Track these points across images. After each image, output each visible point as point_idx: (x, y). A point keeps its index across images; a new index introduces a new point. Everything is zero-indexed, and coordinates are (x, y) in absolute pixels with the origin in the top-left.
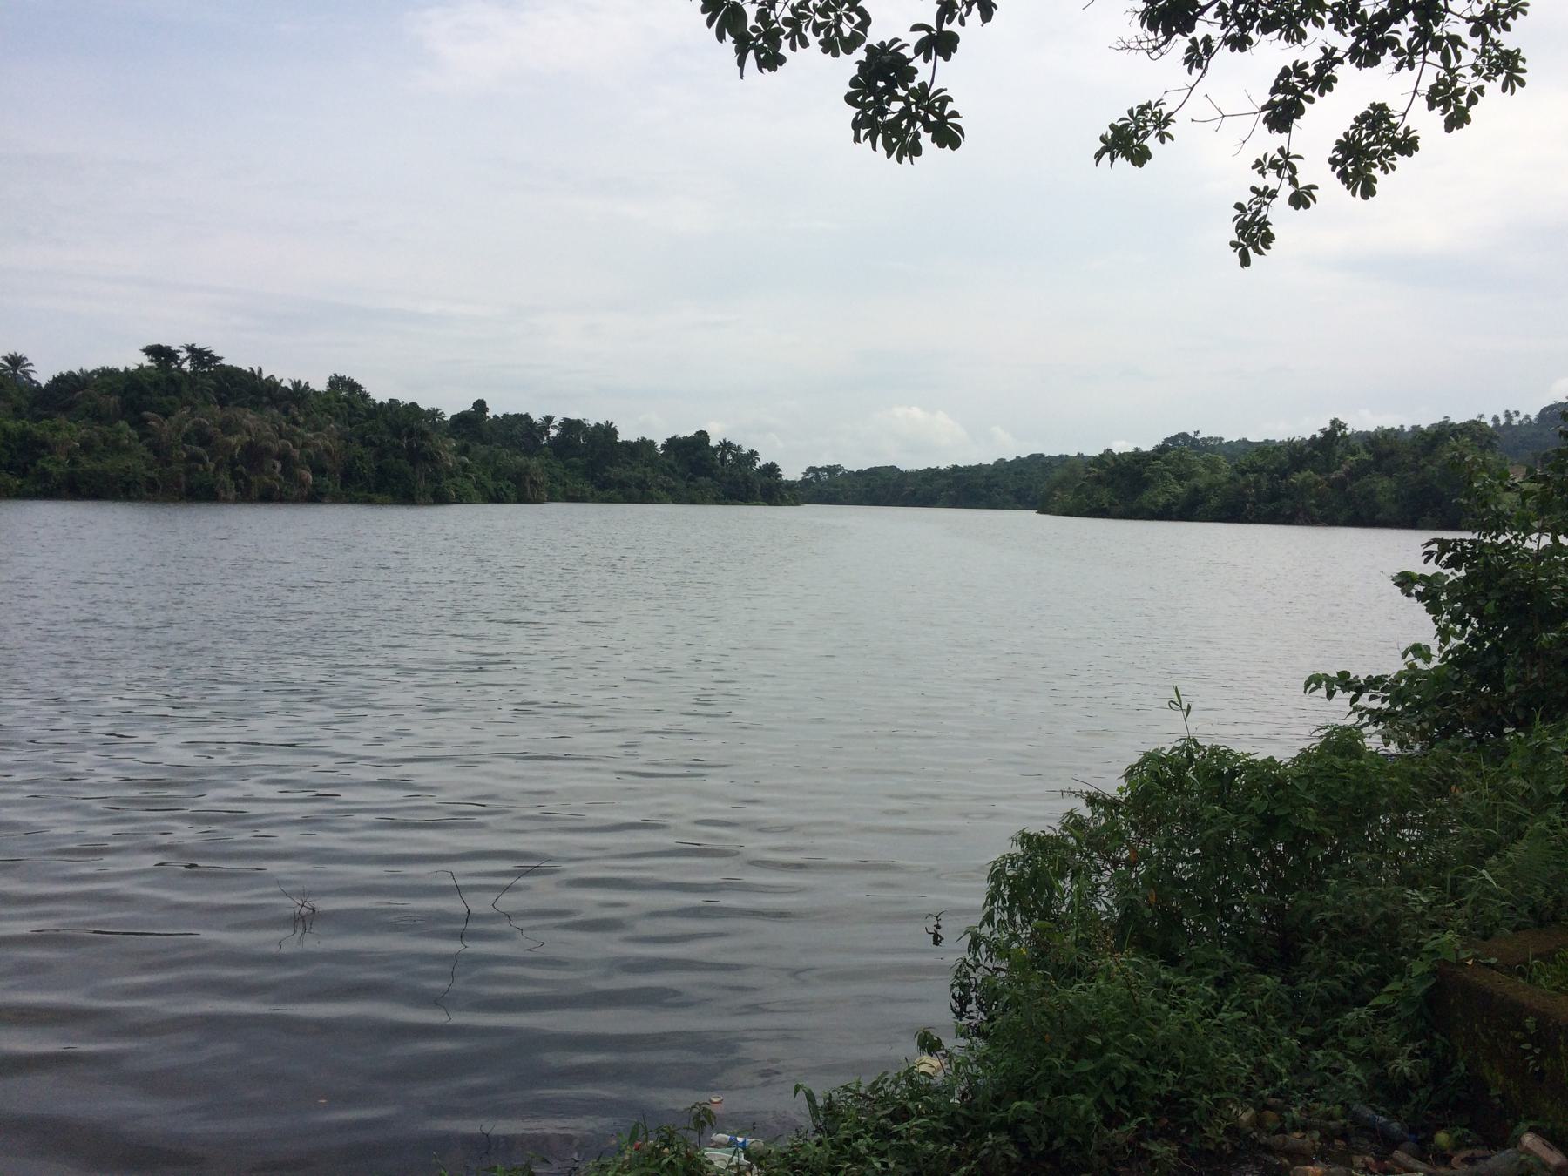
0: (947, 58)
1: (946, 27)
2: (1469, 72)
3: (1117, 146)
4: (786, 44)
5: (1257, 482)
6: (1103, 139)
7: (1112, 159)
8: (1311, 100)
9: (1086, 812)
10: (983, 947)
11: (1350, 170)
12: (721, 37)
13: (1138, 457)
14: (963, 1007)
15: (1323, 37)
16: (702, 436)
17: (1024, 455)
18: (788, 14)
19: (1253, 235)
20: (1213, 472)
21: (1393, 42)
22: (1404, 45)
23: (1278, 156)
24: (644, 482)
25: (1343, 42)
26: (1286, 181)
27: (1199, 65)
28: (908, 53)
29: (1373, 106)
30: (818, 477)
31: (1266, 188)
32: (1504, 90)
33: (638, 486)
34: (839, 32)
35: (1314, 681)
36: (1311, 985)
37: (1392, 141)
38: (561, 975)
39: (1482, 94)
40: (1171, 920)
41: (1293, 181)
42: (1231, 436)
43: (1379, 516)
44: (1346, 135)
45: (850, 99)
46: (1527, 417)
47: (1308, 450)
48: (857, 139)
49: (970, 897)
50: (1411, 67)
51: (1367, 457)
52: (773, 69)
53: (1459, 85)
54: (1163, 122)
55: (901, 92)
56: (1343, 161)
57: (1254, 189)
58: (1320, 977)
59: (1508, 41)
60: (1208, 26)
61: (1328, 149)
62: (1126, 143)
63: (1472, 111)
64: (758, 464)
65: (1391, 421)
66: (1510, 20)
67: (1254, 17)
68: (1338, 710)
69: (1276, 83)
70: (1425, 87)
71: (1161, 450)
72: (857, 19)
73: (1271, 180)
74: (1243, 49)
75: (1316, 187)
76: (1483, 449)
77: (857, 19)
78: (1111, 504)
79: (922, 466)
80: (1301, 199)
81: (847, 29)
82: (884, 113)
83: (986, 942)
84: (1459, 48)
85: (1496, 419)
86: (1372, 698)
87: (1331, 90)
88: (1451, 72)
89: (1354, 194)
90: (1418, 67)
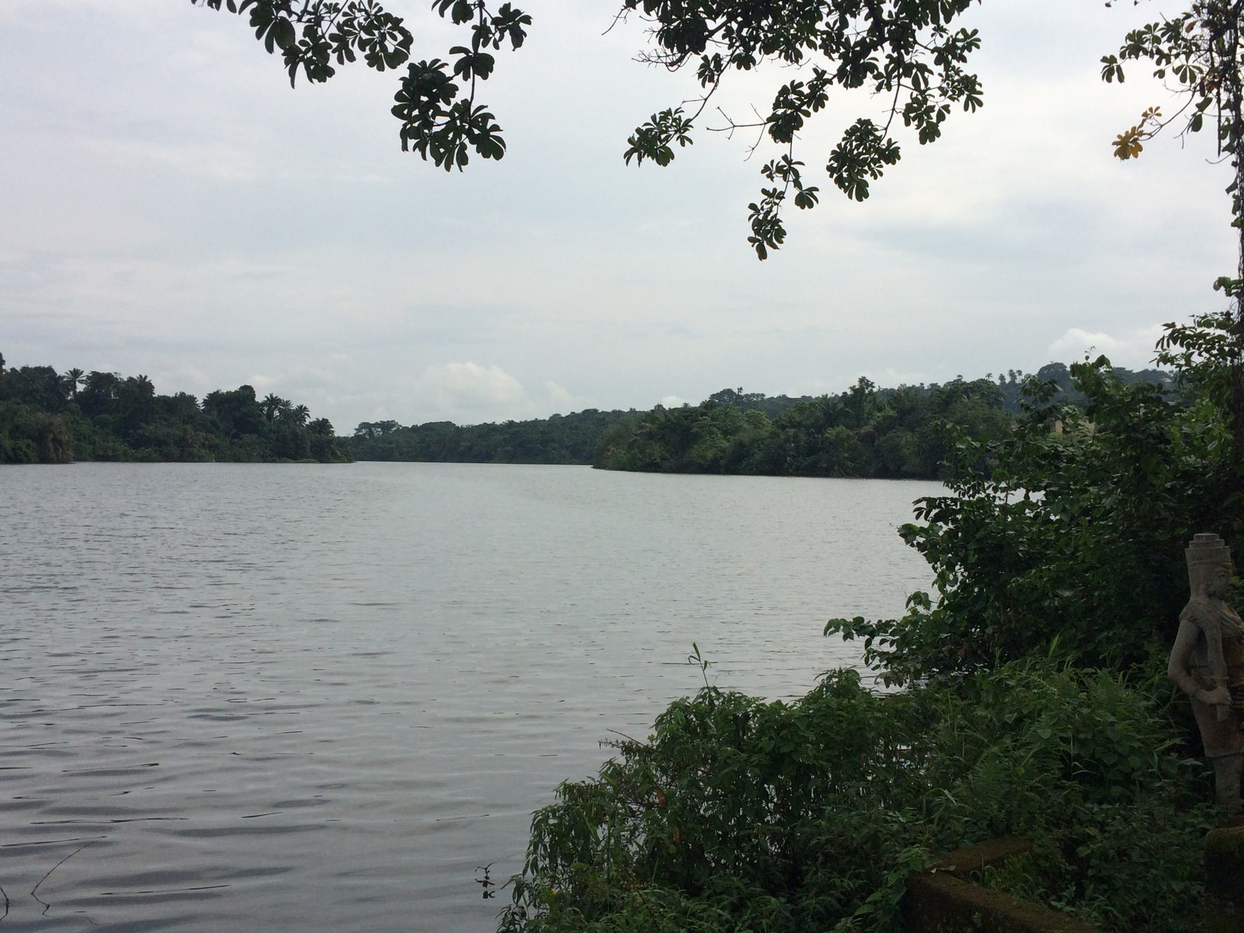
0: (485, 77)
1: (481, 50)
2: (937, 93)
3: (643, 147)
4: (333, 58)
5: (796, 436)
6: (630, 141)
7: (640, 160)
8: (808, 114)
9: (621, 760)
10: (526, 893)
11: (845, 175)
12: (270, 49)
13: (686, 413)
15: (814, 60)
16: (248, 391)
17: (579, 411)
18: (334, 30)
19: (767, 232)
20: (756, 427)
21: (872, 67)
22: (882, 70)
23: (783, 163)
24: (183, 439)
25: (832, 66)
26: (791, 184)
27: (711, 80)
28: (448, 71)
29: (859, 121)
30: (371, 434)
31: (775, 190)
32: (966, 109)
34: (384, 49)
35: (833, 626)
36: (809, 902)
37: (878, 150)
39: (949, 112)
40: (697, 855)
41: (797, 184)
42: (772, 393)
43: (905, 468)
44: (839, 146)
45: (396, 112)
47: (841, 405)
48: (405, 148)
49: (512, 847)
50: (889, 88)
51: (892, 413)
52: (322, 79)
53: (929, 104)
54: (683, 127)
55: (443, 106)
56: (838, 170)
57: (764, 191)
58: (817, 895)
59: (967, 69)
60: (717, 46)
61: (825, 158)
62: (652, 143)
63: (941, 126)
64: (308, 421)
65: (913, 378)
66: (966, 53)
67: (757, 39)
68: (848, 654)
69: (777, 99)
70: (901, 106)
71: (708, 406)
72: (400, 38)
73: (779, 183)
74: (748, 68)
75: (817, 190)
76: (991, 405)
77: (400, 38)
78: (663, 459)
79: (477, 422)
80: (805, 199)
81: (391, 45)
82: (430, 125)
83: (530, 889)
84: (926, 74)
85: (1002, 378)
86: (882, 642)
87: (823, 106)
88: (922, 93)
89: (850, 197)
90: (894, 89)
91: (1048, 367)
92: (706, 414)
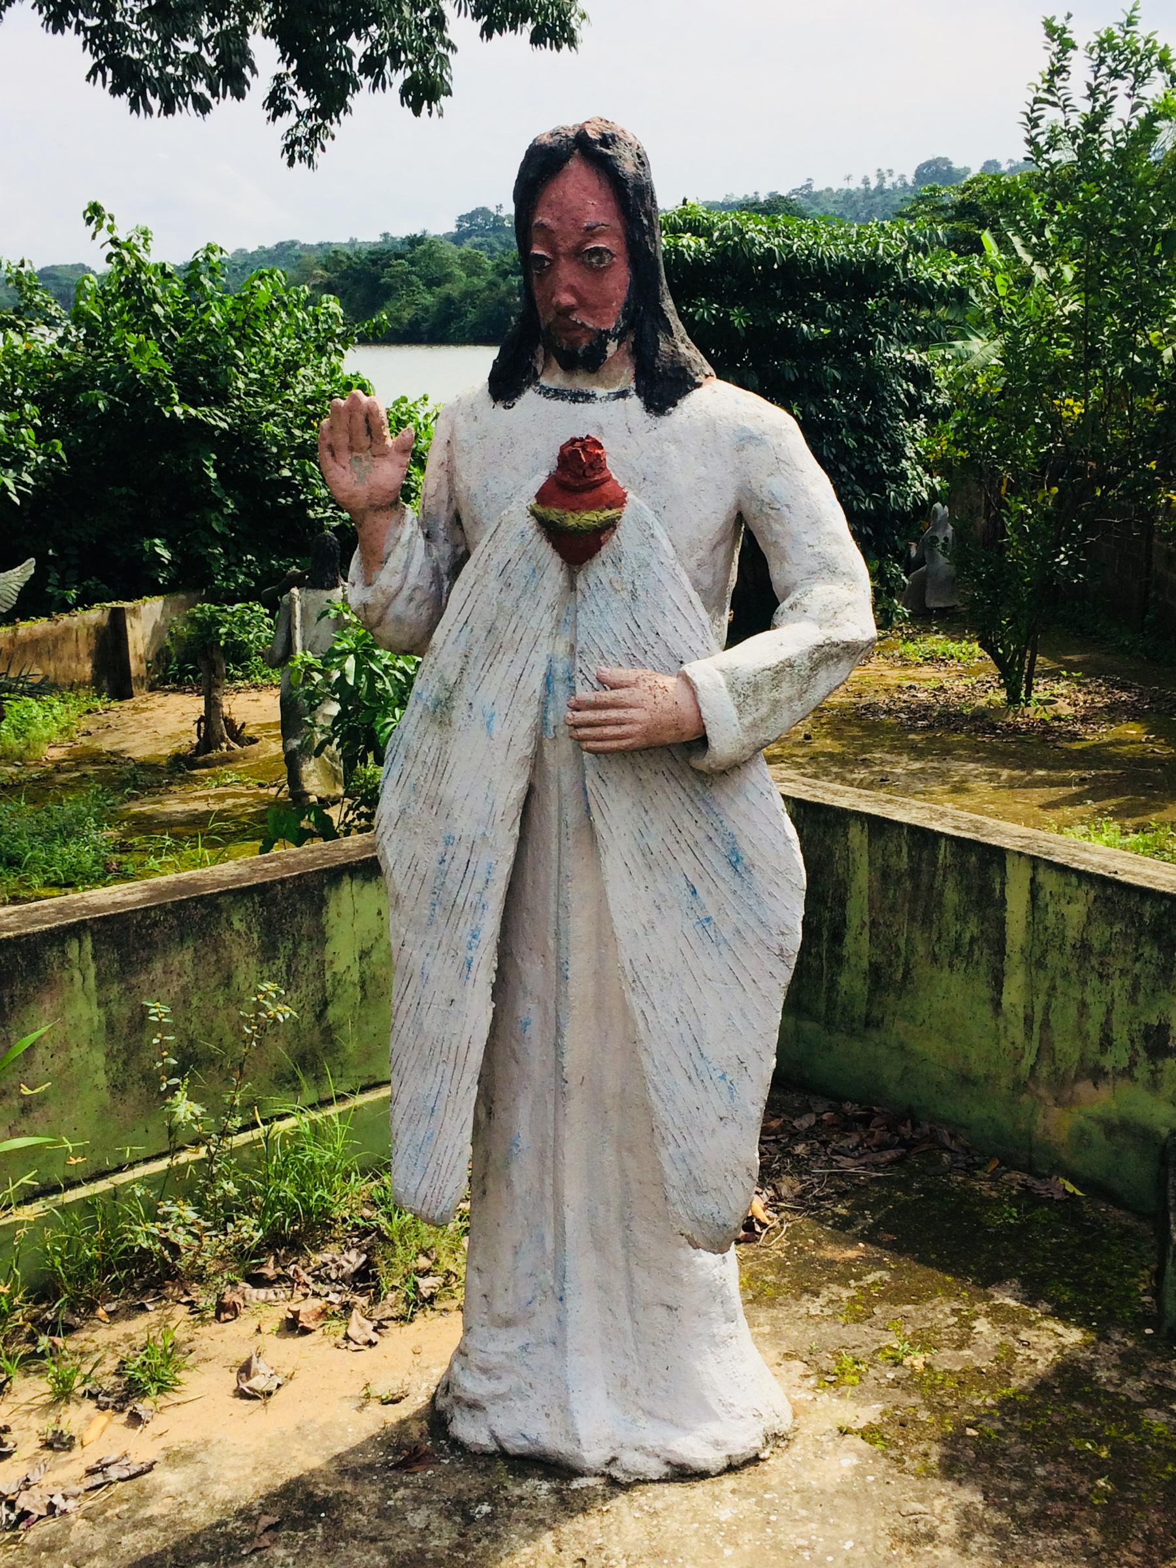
46: (902, 177)
85: (866, 181)
91: (928, 165)
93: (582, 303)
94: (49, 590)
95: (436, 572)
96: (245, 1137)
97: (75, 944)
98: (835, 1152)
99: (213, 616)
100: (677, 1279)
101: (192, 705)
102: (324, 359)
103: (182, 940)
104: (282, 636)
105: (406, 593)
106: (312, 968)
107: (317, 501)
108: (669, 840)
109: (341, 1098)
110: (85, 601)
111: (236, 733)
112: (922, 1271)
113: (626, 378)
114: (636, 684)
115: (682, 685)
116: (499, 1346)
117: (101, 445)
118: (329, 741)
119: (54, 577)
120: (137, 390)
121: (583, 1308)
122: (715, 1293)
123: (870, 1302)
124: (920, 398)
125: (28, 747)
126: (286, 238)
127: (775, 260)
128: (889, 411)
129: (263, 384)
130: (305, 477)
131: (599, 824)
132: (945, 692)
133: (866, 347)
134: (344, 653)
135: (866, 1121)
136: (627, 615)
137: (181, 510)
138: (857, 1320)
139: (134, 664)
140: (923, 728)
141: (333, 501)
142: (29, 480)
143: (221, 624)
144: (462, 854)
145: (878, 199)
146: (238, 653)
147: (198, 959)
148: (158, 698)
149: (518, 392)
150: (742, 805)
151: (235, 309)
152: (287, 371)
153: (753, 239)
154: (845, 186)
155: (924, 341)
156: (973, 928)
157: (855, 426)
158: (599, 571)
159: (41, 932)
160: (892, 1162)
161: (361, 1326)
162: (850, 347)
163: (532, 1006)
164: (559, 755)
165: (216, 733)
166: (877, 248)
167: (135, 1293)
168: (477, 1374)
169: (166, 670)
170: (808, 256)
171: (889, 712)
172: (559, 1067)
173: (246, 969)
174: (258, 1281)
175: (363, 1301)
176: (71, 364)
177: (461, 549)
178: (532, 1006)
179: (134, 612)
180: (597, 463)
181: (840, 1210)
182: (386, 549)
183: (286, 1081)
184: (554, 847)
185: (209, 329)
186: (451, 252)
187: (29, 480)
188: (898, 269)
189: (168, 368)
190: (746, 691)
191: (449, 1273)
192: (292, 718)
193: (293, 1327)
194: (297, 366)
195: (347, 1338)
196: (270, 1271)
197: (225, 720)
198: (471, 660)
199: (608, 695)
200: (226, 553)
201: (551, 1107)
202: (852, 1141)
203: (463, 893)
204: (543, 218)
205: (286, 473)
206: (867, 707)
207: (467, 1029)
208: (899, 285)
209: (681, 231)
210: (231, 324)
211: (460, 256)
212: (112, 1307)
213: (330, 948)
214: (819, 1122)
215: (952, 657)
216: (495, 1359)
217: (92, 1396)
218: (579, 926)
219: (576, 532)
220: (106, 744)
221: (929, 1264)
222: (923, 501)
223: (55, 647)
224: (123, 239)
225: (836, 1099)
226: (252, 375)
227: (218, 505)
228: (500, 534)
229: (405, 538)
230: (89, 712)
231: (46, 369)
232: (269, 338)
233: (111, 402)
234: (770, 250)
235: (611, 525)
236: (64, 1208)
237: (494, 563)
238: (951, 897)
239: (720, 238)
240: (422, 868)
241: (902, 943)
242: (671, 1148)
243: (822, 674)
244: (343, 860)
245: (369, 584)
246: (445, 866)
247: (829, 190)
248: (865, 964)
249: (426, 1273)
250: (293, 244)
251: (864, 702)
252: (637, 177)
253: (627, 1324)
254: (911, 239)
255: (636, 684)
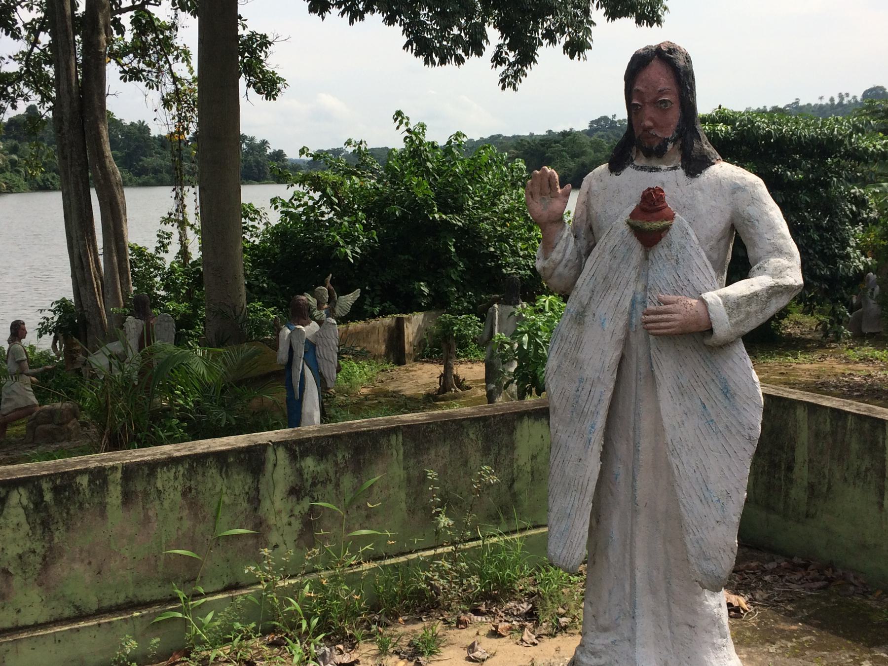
14: (330, 641)
33: (167, 172)
38: (670, 330)
46: (855, 97)
64: (269, 151)
85: (832, 99)
91: (870, 90)
92: (558, 142)
93: (656, 125)
94: (365, 307)
95: (579, 253)
96: (474, 543)
97: (394, 437)
98: (787, 581)
99: (451, 321)
100: (695, 612)
101: (438, 369)
102: (514, 191)
103: (445, 441)
104: (488, 330)
105: (564, 262)
106: (507, 462)
107: (508, 265)
108: (692, 381)
109: (523, 530)
110: (384, 313)
111: (460, 383)
112: (834, 638)
113: (677, 160)
114: (677, 302)
115: (701, 304)
116: (600, 641)
117: (396, 234)
118: (512, 381)
119: (368, 301)
120: (416, 206)
121: (645, 625)
122: (715, 621)
123: (803, 649)
124: (859, 214)
125: (351, 387)
126: (495, 133)
127: (772, 137)
128: (840, 220)
129: (481, 203)
130: (502, 252)
131: (657, 373)
132: (872, 377)
133: (826, 185)
134: (523, 333)
135: (805, 567)
136: (674, 271)
137: (435, 266)
138: (796, 656)
139: (407, 347)
140: (857, 396)
141: (516, 265)
142: (359, 251)
143: (455, 325)
144: (588, 386)
145: (840, 109)
146: (462, 343)
147: (452, 451)
148: (419, 365)
149: (623, 168)
150: (730, 364)
151: (469, 165)
152: (495, 197)
153: (759, 126)
154: (819, 102)
155: (864, 182)
156: (867, 463)
157: (818, 228)
158: (660, 250)
159: (379, 429)
160: (819, 588)
161: (529, 636)
162: (817, 184)
163: (621, 466)
164: (637, 340)
165: (449, 385)
166: (834, 130)
167: (416, 613)
168: (589, 655)
169: (423, 351)
170: (792, 135)
171: (836, 387)
172: (634, 497)
173: (475, 458)
174: (477, 612)
175: (529, 625)
176: (382, 193)
177: (591, 244)
178: (621, 466)
179: (409, 320)
180: (661, 199)
181: (789, 608)
182: (555, 242)
183: (494, 519)
184: (634, 385)
185: (455, 175)
186: (586, 140)
187: (359, 251)
188: (846, 142)
189: (432, 195)
190: (733, 306)
191: (575, 617)
192: (492, 374)
193: (495, 634)
194: (501, 194)
195: (522, 640)
196: (483, 608)
197: (455, 376)
198: (595, 293)
199: (663, 307)
200: (458, 290)
201: (629, 518)
202: (798, 576)
203: (587, 406)
204: (639, 87)
205: (492, 249)
206: (823, 384)
207: (588, 473)
208: (846, 151)
209: (717, 122)
210: (467, 172)
211: (591, 142)
212: (406, 618)
213: (516, 452)
214: (779, 567)
215: (877, 359)
216: (599, 648)
217: (397, 653)
218: (646, 424)
219: (650, 231)
220: (391, 387)
221: (839, 635)
222: (860, 270)
223: (367, 336)
224: (412, 129)
225: (789, 557)
226: (476, 199)
227: (455, 265)
228: (612, 232)
229: (565, 236)
230: (383, 371)
231: (370, 195)
232: (485, 179)
233: (402, 211)
234: (769, 132)
235: (667, 228)
236: (384, 567)
237: (608, 247)
238: (855, 446)
239: (739, 126)
240: (567, 393)
241: (827, 472)
242: (691, 536)
243: (774, 301)
244: (524, 409)
245: (546, 259)
246: (578, 393)
247: (809, 105)
248: (805, 483)
249: (563, 616)
250: (500, 136)
251: (821, 381)
252: (685, 67)
253: (668, 633)
254: (854, 126)
255: (677, 302)
